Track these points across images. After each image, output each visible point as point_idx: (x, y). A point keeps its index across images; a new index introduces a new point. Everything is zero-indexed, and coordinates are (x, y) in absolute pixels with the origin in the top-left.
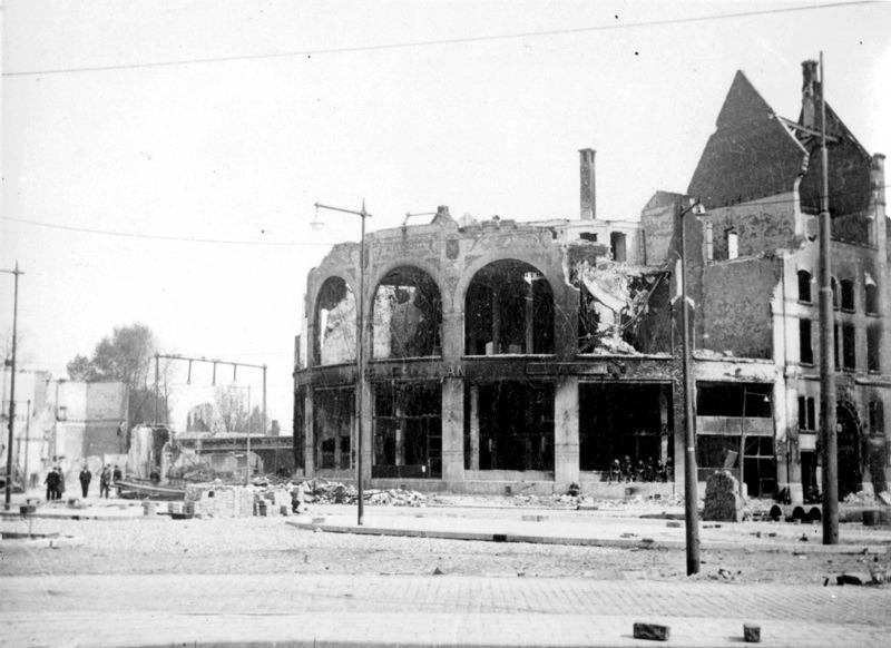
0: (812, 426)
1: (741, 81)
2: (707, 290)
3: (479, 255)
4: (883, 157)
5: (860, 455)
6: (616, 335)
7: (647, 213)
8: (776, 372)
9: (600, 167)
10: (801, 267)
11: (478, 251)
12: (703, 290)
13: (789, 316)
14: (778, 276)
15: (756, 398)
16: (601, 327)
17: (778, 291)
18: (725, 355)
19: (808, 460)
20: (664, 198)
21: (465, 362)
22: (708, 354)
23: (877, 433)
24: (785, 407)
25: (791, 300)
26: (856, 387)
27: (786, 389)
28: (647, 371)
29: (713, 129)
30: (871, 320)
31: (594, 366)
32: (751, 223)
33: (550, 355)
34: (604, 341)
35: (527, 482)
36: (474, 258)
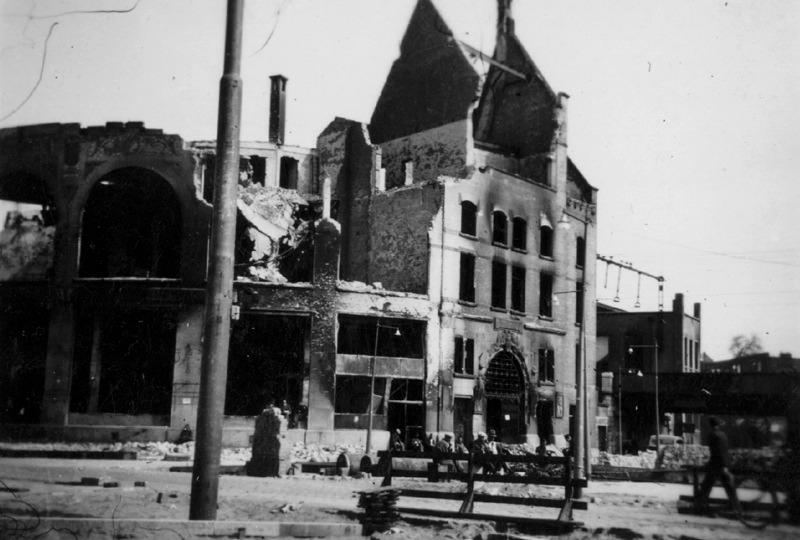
0: (470, 370)
2: (373, 220)
4: (567, 97)
5: (526, 403)
6: (271, 265)
7: (323, 140)
8: (431, 309)
9: (291, 95)
10: (467, 197)
12: (369, 221)
13: (449, 248)
14: (437, 203)
15: (410, 337)
17: (437, 221)
18: (375, 288)
19: (464, 407)
20: (339, 125)
22: (357, 285)
23: (547, 382)
24: (439, 348)
26: (525, 331)
27: (441, 327)
28: (283, 300)
30: (545, 264)
32: (427, 154)
34: (253, 270)
35: (138, 427)
36: (97, 164)
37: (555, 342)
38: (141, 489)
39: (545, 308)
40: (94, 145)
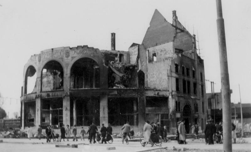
1: (157, 12)
3: (77, 56)
8: (169, 94)
11: (76, 55)
16: (116, 81)
21: (70, 91)
24: (172, 104)
25: (173, 72)
29: (149, 26)
31: (113, 92)
33: (98, 88)
36: (74, 57)
37: (198, 102)
38: (57, 145)
39: (195, 93)
40: (74, 52)
